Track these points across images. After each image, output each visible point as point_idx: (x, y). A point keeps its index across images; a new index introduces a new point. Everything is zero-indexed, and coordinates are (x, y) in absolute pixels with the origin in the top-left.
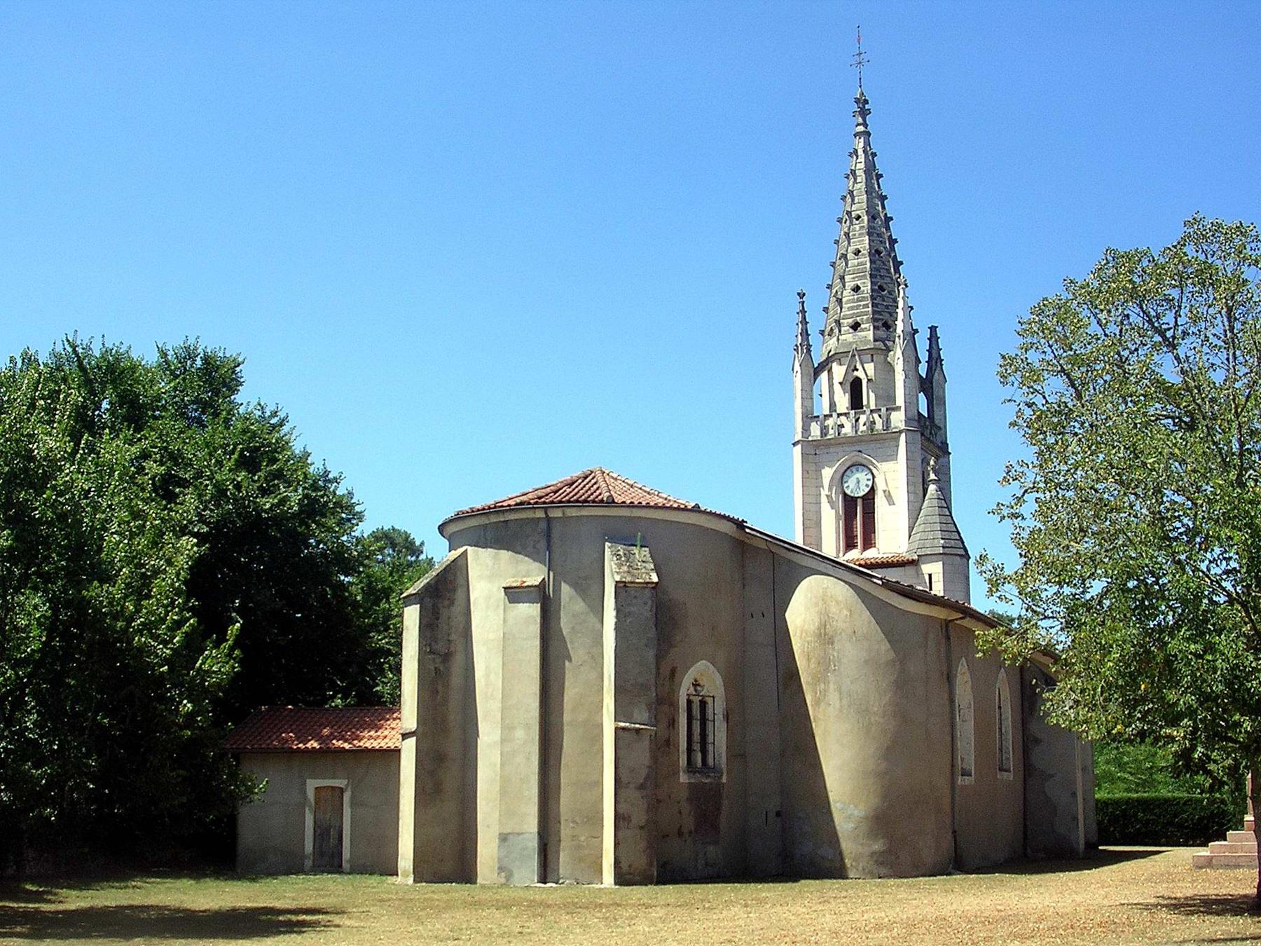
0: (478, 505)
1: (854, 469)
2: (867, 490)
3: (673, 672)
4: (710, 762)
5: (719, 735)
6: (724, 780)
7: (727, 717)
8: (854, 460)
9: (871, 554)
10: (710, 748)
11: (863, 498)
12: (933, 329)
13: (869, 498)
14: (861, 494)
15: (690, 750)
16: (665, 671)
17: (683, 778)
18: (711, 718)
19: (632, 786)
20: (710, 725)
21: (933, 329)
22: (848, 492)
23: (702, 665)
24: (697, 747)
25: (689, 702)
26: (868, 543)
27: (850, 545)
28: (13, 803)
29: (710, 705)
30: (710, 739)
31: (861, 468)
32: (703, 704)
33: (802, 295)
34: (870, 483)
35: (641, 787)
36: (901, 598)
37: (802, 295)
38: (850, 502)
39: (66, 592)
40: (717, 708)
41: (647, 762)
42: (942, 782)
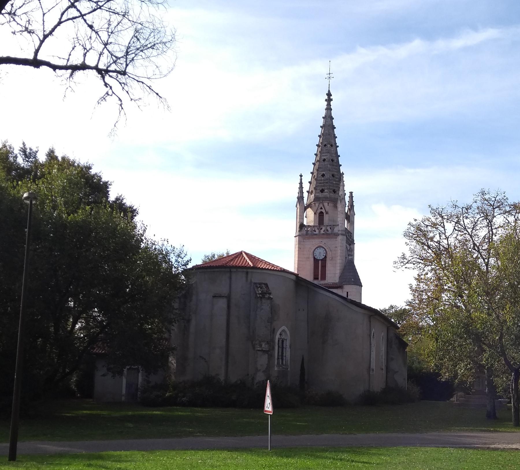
0: (48, 68)
2: (323, 257)
3: (274, 329)
5: (288, 353)
7: (290, 347)
9: (322, 282)
10: (284, 358)
11: (322, 260)
12: (351, 193)
13: (324, 260)
14: (321, 258)
15: (278, 358)
17: (276, 369)
20: (284, 350)
21: (351, 193)
22: (316, 257)
23: (284, 327)
25: (279, 341)
26: (324, 277)
27: (316, 278)
28: (163, 269)
29: (285, 342)
33: (301, 176)
35: (264, 372)
37: (301, 176)
38: (316, 261)
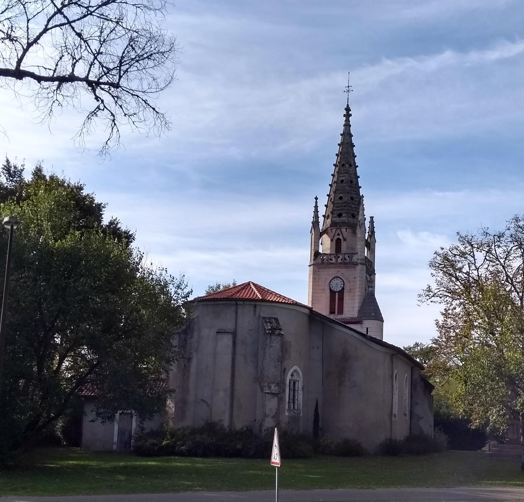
1: (335, 279)
2: (341, 289)
3: (285, 369)
4: (296, 407)
5: (300, 396)
6: (301, 415)
7: (303, 389)
8: (336, 275)
9: (339, 317)
10: (296, 402)
11: (339, 292)
12: (372, 218)
13: (341, 292)
14: (338, 290)
15: (289, 402)
16: (283, 369)
17: (287, 414)
18: (297, 389)
19: (270, 416)
20: (296, 393)
21: (372, 218)
22: (332, 289)
24: (291, 401)
25: (290, 382)
26: (341, 311)
27: (332, 312)
30: (296, 398)
31: (339, 279)
32: (294, 383)
34: (342, 286)
36: (376, 345)
39: (136, 290)
40: (300, 385)
41: (276, 407)
42: (240, 311)
